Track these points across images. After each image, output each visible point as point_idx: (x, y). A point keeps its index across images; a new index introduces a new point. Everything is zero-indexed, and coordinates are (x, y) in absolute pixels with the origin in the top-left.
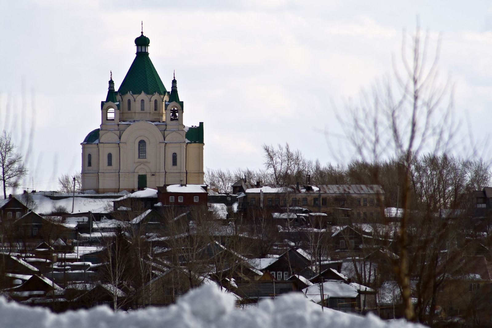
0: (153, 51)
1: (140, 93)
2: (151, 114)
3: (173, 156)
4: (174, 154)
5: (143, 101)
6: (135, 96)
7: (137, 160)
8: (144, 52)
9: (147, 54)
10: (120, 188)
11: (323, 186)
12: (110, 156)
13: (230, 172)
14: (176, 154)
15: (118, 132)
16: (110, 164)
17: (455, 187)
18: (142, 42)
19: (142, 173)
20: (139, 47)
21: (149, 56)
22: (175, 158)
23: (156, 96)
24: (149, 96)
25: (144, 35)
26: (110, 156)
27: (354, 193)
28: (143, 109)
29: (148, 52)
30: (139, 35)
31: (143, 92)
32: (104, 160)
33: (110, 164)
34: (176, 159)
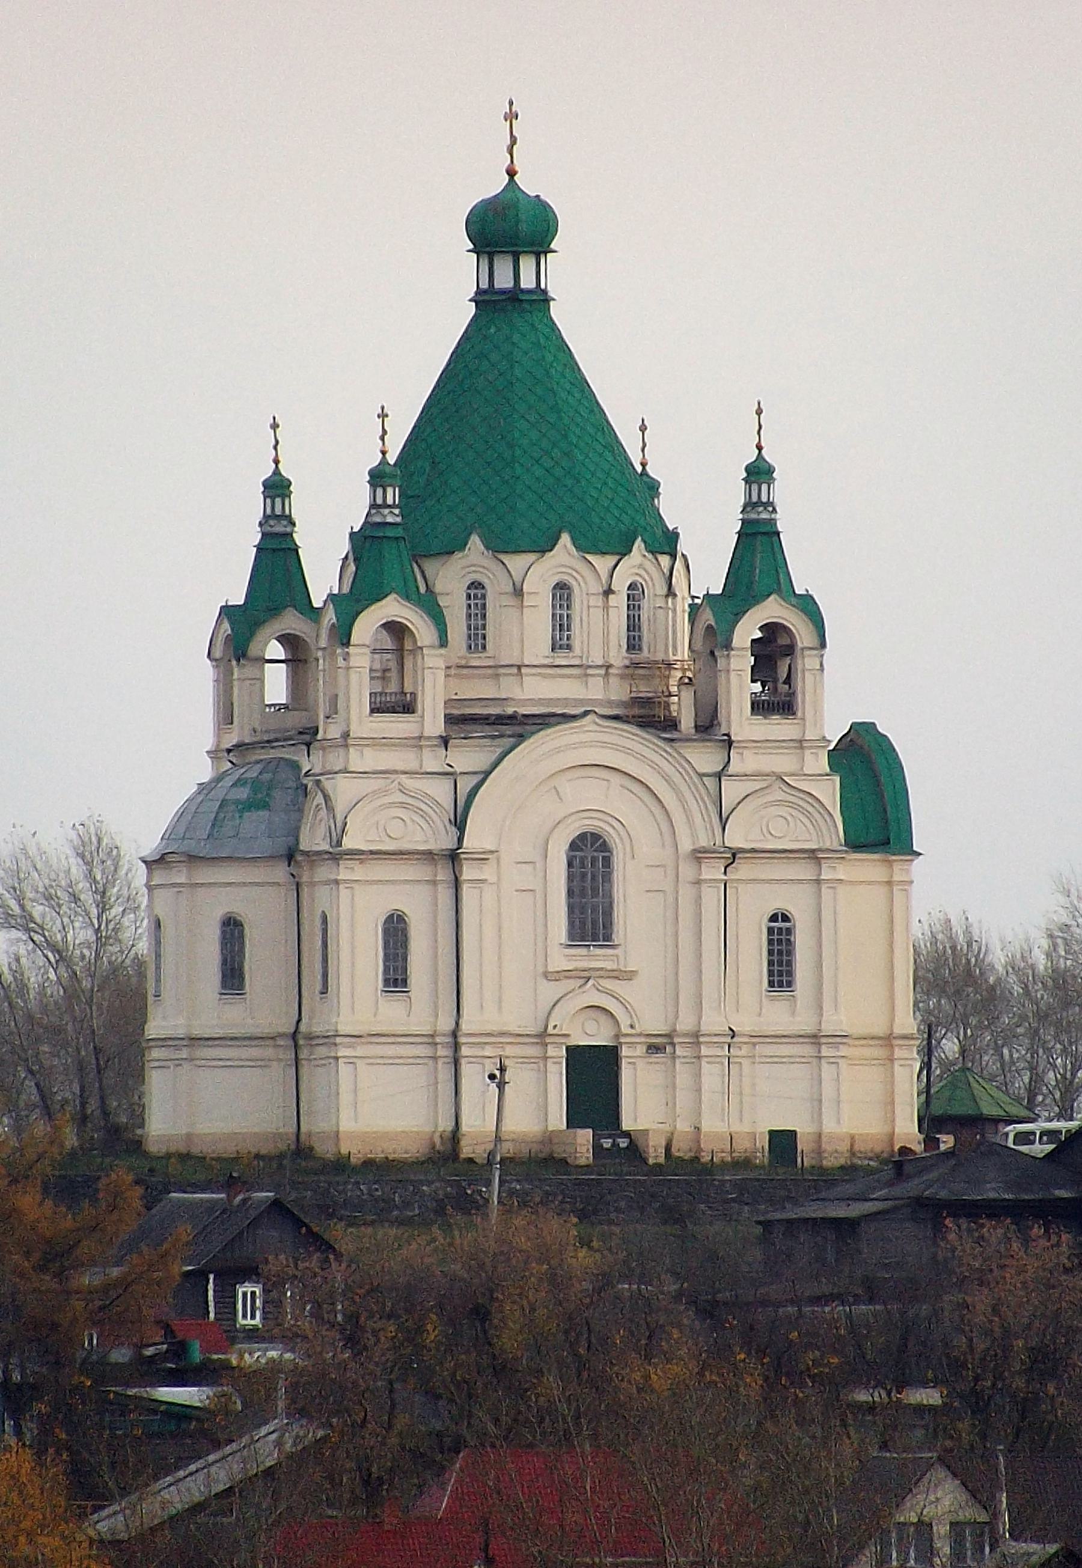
0: (581, 293)
1: (545, 546)
2: (611, 671)
3: (770, 931)
4: (774, 918)
5: (562, 591)
6: (516, 563)
7: (563, 958)
8: (529, 292)
9: (541, 299)
10: (465, 1128)
11: (249, 786)
12: (395, 931)
13: (42, 845)
14: (786, 918)
15: (441, 791)
16: (396, 979)
17: (604, 1281)
18: (509, 229)
19: (594, 1035)
20: (533, 285)
21: (556, 311)
22: (780, 942)
23: (637, 563)
24: (602, 563)
25: (527, 184)
26: (395, 931)
27: (705, 779)
28: (561, 642)
29: (549, 288)
30: (495, 185)
31: (565, 539)
32: (359, 956)
33: (396, 979)
34: (790, 953)
